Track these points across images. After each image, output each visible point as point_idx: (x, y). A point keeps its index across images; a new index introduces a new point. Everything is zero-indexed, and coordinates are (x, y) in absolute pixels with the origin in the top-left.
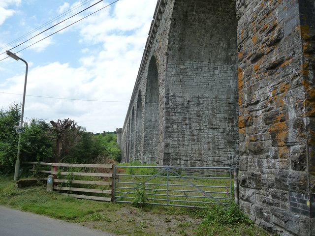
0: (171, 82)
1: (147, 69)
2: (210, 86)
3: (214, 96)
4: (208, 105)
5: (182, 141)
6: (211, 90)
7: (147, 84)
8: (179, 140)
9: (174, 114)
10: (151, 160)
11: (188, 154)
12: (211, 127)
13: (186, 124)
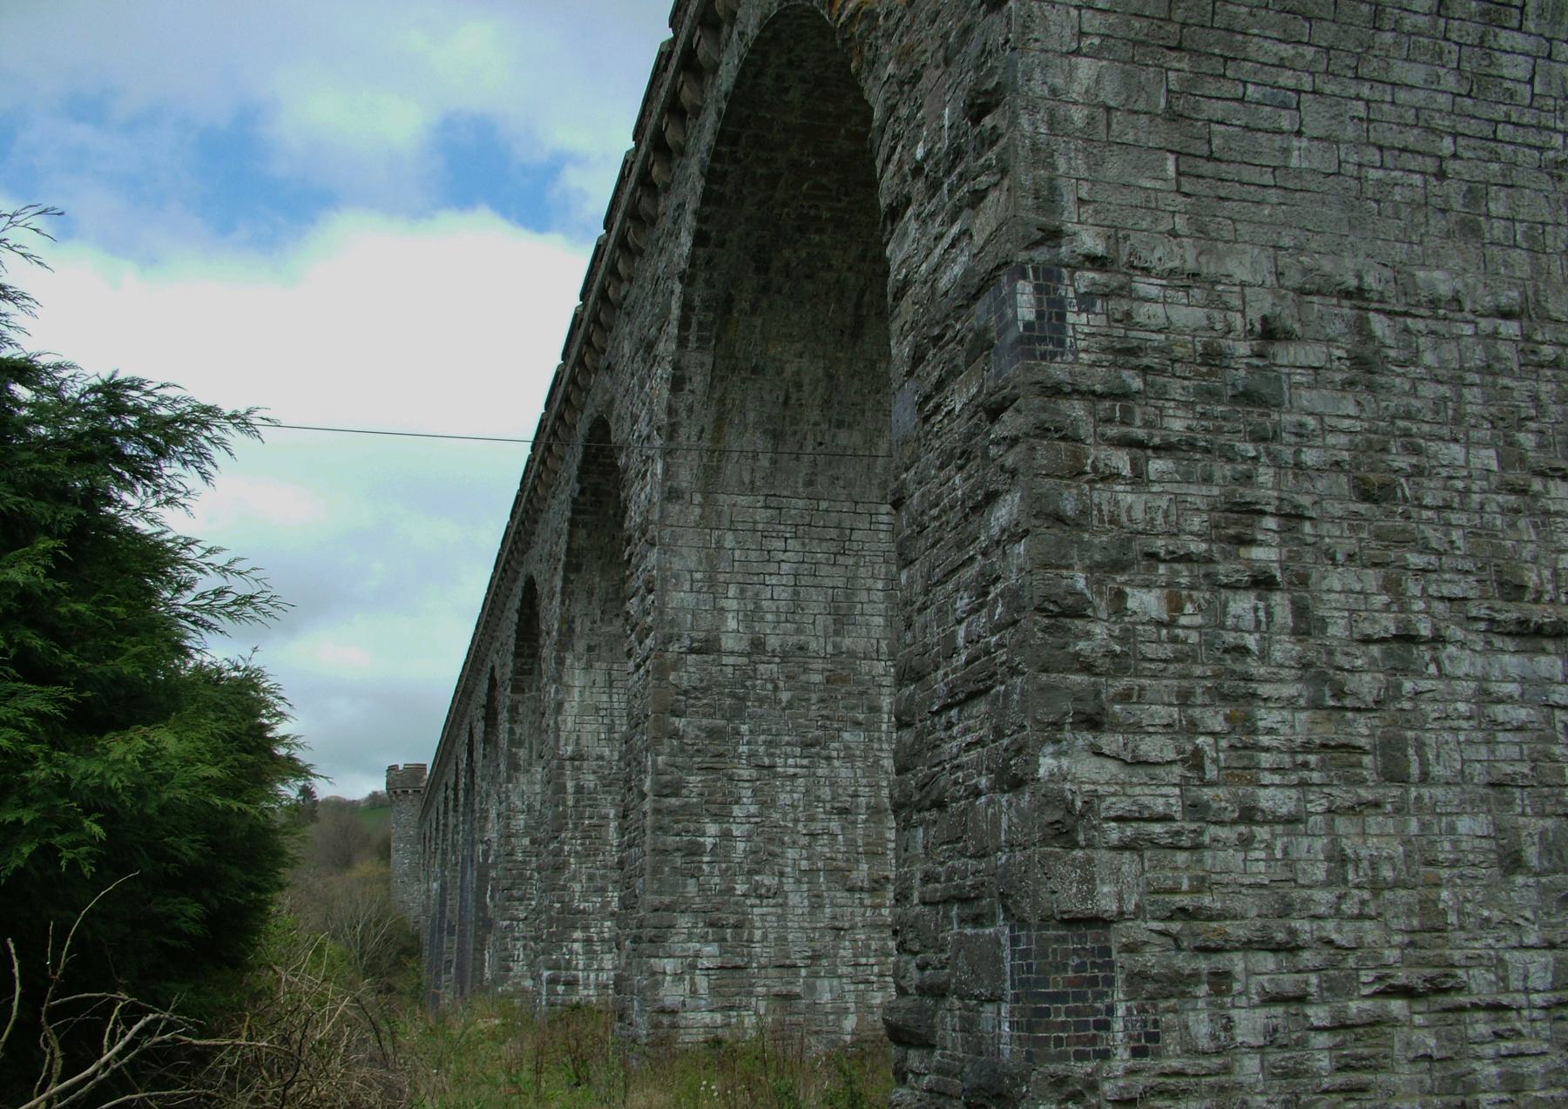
0: (1078, 116)
1: (690, 185)
2: (1453, 192)
3: (1510, 297)
4: (1458, 382)
5: (1231, 776)
6: (1470, 229)
7: (684, 324)
8: (1195, 761)
9: (1121, 461)
10: (714, 990)
11: (1303, 926)
12: (1509, 613)
13: (1262, 583)
